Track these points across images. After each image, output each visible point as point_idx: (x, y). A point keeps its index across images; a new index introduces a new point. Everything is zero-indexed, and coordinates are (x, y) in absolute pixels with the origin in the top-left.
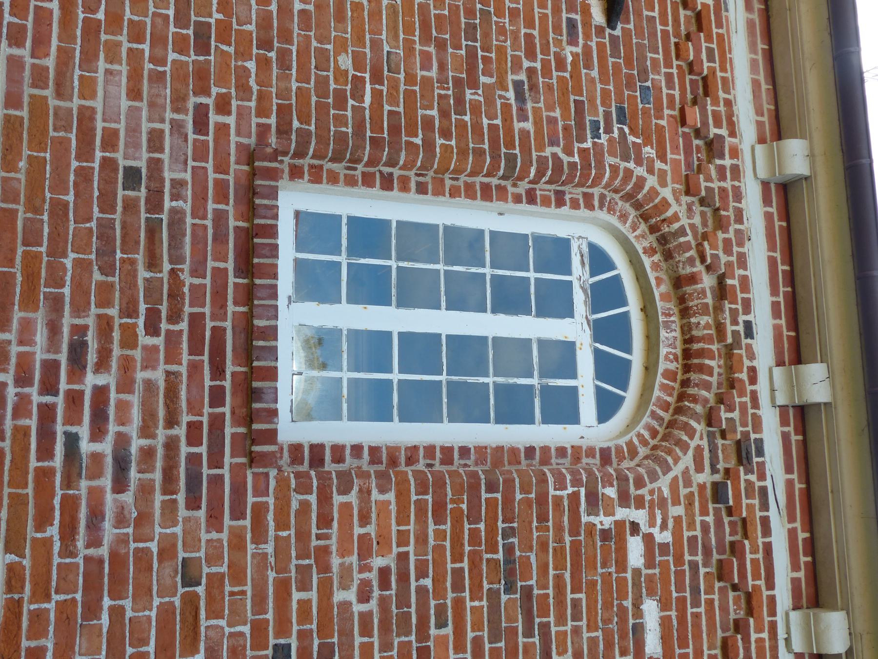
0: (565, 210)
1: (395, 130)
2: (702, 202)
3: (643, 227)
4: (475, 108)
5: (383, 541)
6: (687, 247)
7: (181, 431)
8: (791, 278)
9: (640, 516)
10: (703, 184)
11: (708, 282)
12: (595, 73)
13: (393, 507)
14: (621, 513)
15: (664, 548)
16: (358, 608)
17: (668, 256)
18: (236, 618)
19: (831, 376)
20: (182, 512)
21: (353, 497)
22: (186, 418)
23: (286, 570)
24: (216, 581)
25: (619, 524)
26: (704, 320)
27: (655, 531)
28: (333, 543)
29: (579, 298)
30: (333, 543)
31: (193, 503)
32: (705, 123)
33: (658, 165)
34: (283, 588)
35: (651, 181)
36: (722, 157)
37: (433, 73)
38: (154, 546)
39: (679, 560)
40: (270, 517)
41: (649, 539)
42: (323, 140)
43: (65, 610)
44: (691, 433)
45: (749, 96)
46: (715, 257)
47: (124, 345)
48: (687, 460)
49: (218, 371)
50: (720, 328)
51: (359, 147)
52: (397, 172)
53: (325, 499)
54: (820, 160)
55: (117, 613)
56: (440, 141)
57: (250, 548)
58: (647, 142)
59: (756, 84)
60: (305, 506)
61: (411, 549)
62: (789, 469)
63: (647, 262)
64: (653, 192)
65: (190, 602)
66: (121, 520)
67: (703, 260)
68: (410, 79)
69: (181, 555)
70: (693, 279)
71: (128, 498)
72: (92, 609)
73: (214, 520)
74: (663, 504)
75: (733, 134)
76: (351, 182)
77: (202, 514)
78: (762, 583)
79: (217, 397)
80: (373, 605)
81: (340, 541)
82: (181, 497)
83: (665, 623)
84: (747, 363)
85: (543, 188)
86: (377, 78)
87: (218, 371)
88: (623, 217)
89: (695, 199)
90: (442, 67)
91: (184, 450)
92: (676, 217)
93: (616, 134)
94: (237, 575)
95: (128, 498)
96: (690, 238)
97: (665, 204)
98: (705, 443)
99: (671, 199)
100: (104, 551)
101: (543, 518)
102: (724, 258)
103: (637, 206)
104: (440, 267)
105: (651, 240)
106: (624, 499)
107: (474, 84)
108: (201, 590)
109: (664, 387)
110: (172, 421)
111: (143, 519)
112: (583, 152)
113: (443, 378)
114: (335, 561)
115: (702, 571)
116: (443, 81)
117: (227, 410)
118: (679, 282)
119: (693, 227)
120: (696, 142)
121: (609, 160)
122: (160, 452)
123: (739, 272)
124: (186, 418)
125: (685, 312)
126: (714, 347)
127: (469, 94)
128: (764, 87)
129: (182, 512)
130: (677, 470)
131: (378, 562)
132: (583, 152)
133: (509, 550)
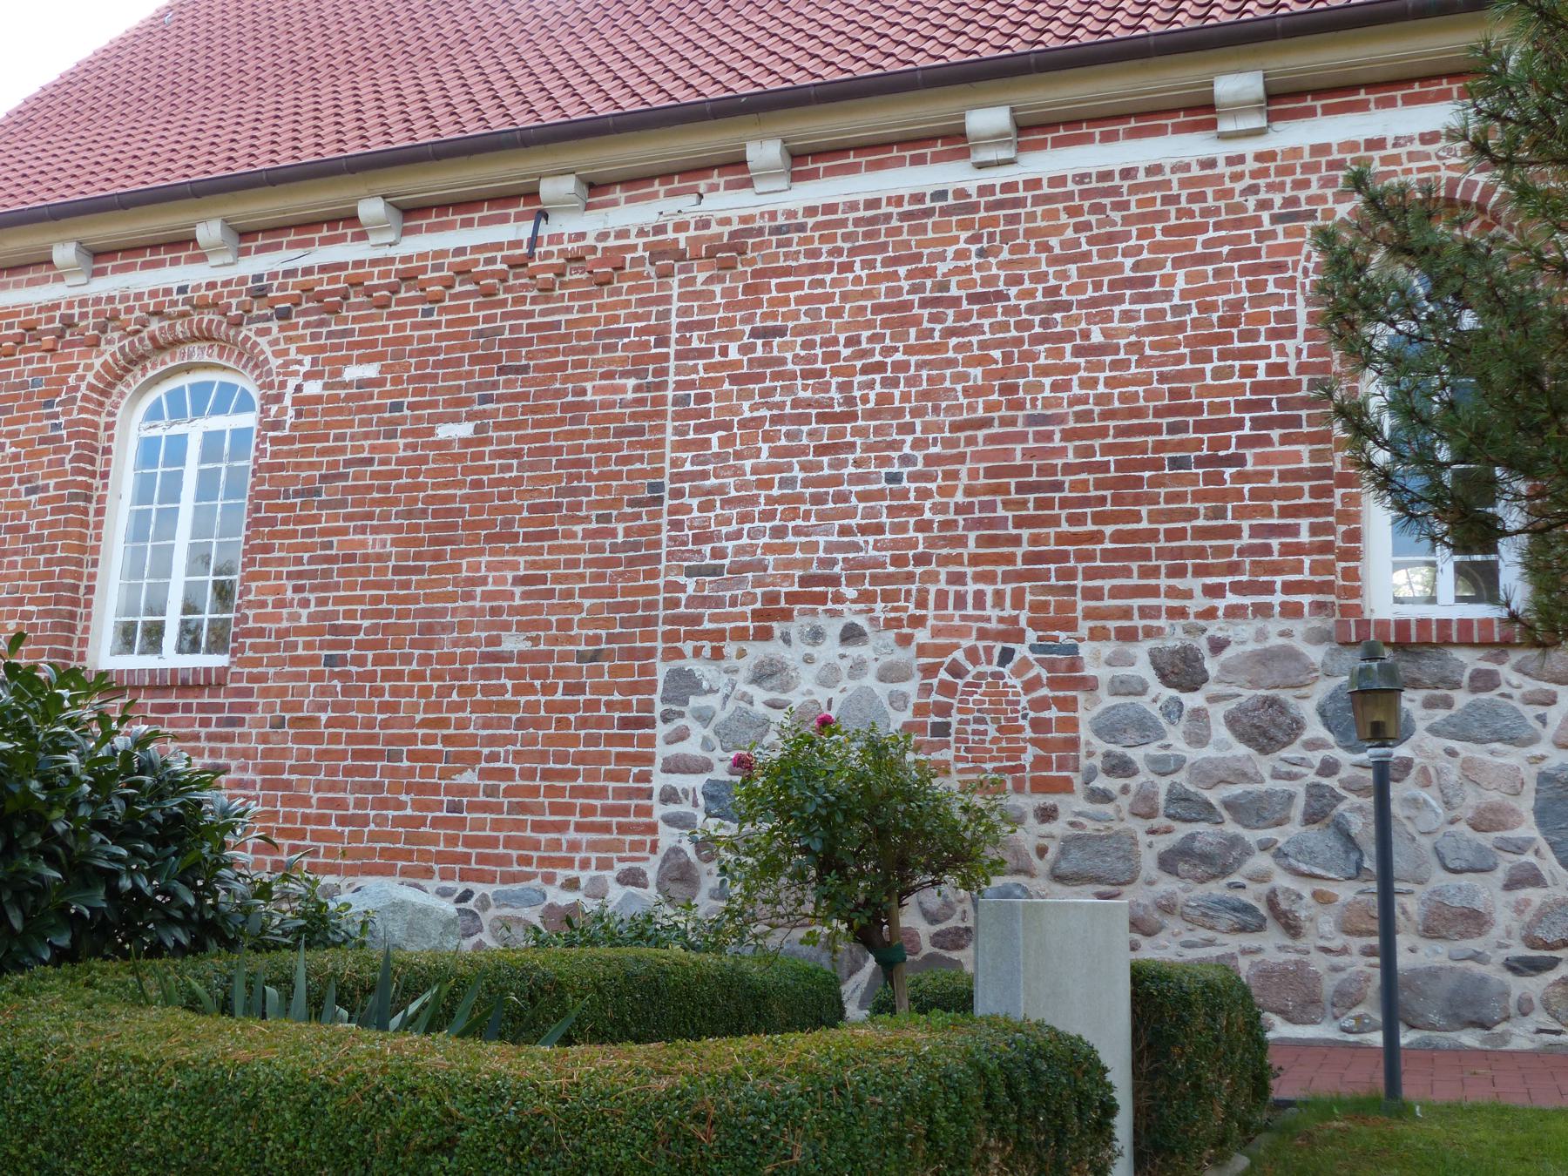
0: (114, 446)
1: (50, 588)
2: (104, 331)
3: (129, 378)
4: (41, 526)
5: (279, 590)
6: (132, 343)
7: (203, 731)
8: (155, 247)
9: (292, 383)
10: (91, 332)
11: (155, 325)
12: (22, 427)
13: (260, 583)
14: (287, 401)
15: (314, 362)
16: (312, 608)
17: (143, 357)
18: (304, 692)
19: (204, 221)
20: (245, 729)
21: (250, 613)
22: (197, 728)
23: (284, 659)
24: (286, 707)
25: (295, 402)
26: (178, 328)
27: (303, 370)
28: (274, 626)
29: (177, 430)
30: (274, 626)
31: (241, 723)
32: (52, 331)
33: (80, 371)
34: (296, 661)
35: (90, 378)
36: (72, 316)
37: (19, 559)
38: (261, 747)
39: (322, 349)
40: (255, 670)
41: (308, 376)
42: (55, 640)
43: (287, 801)
44: (247, 338)
45: (46, 287)
46: (137, 321)
47: (632, 843)
48: (263, 342)
49: (172, 708)
50: (183, 315)
51: (59, 614)
52: (85, 582)
53: (248, 633)
54: (63, 236)
55: (293, 770)
56: (59, 554)
57: (270, 683)
58: (64, 381)
59: (31, 283)
60: (253, 647)
61: (285, 569)
62: (278, 247)
63: (151, 373)
64: (98, 376)
65: (295, 722)
66: (244, 769)
67: (138, 332)
68: (22, 576)
69: (267, 729)
70: (153, 338)
71: (234, 764)
72: (287, 785)
73: (251, 708)
74: (286, 364)
75: (57, 306)
76: (89, 617)
77: (247, 716)
78: (343, 274)
79: (187, 708)
80: (312, 597)
81: (273, 621)
82: (237, 730)
83: (362, 360)
84: (203, 292)
85: (99, 467)
86: (20, 602)
87: (172, 708)
88: (122, 395)
89: (103, 337)
90: (16, 552)
91: (213, 729)
92: (113, 355)
93: (59, 409)
94: (282, 692)
95: (234, 764)
96: (126, 342)
97: (105, 365)
98: (254, 327)
99: (101, 360)
100: (258, 778)
101: (282, 467)
102: (137, 313)
103: (112, 385)
104: (149, 545)
105: (137, 370)
106: (278, 399)
107: (26, 528)
108: (287, 716)
109: (228, 359)
110: (196, 737)
111: (246, 754)
112: (70, 436)
113: (214, 541)
114: (285, 624)
115: (333, 328)
116: (23, 552)
117: (195, 701)
118: (159, 348)
119: (121, 339)
120: (68, 337)
121: (75, 416)
122: (212, 744)
123: (146, 300)
124: (197, 728)
125: (177, 342)
126: (196, 318)
127: (32, 531)
128: (31, 275)
129: (245, 729)
130: (268, 350)
131: (289, 594)
132: (70, 436)
133: (297, 494)
